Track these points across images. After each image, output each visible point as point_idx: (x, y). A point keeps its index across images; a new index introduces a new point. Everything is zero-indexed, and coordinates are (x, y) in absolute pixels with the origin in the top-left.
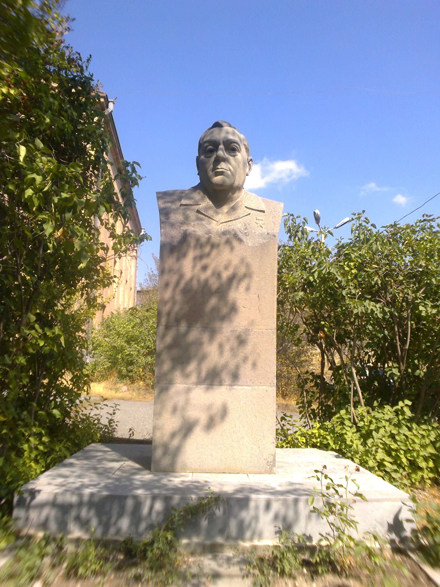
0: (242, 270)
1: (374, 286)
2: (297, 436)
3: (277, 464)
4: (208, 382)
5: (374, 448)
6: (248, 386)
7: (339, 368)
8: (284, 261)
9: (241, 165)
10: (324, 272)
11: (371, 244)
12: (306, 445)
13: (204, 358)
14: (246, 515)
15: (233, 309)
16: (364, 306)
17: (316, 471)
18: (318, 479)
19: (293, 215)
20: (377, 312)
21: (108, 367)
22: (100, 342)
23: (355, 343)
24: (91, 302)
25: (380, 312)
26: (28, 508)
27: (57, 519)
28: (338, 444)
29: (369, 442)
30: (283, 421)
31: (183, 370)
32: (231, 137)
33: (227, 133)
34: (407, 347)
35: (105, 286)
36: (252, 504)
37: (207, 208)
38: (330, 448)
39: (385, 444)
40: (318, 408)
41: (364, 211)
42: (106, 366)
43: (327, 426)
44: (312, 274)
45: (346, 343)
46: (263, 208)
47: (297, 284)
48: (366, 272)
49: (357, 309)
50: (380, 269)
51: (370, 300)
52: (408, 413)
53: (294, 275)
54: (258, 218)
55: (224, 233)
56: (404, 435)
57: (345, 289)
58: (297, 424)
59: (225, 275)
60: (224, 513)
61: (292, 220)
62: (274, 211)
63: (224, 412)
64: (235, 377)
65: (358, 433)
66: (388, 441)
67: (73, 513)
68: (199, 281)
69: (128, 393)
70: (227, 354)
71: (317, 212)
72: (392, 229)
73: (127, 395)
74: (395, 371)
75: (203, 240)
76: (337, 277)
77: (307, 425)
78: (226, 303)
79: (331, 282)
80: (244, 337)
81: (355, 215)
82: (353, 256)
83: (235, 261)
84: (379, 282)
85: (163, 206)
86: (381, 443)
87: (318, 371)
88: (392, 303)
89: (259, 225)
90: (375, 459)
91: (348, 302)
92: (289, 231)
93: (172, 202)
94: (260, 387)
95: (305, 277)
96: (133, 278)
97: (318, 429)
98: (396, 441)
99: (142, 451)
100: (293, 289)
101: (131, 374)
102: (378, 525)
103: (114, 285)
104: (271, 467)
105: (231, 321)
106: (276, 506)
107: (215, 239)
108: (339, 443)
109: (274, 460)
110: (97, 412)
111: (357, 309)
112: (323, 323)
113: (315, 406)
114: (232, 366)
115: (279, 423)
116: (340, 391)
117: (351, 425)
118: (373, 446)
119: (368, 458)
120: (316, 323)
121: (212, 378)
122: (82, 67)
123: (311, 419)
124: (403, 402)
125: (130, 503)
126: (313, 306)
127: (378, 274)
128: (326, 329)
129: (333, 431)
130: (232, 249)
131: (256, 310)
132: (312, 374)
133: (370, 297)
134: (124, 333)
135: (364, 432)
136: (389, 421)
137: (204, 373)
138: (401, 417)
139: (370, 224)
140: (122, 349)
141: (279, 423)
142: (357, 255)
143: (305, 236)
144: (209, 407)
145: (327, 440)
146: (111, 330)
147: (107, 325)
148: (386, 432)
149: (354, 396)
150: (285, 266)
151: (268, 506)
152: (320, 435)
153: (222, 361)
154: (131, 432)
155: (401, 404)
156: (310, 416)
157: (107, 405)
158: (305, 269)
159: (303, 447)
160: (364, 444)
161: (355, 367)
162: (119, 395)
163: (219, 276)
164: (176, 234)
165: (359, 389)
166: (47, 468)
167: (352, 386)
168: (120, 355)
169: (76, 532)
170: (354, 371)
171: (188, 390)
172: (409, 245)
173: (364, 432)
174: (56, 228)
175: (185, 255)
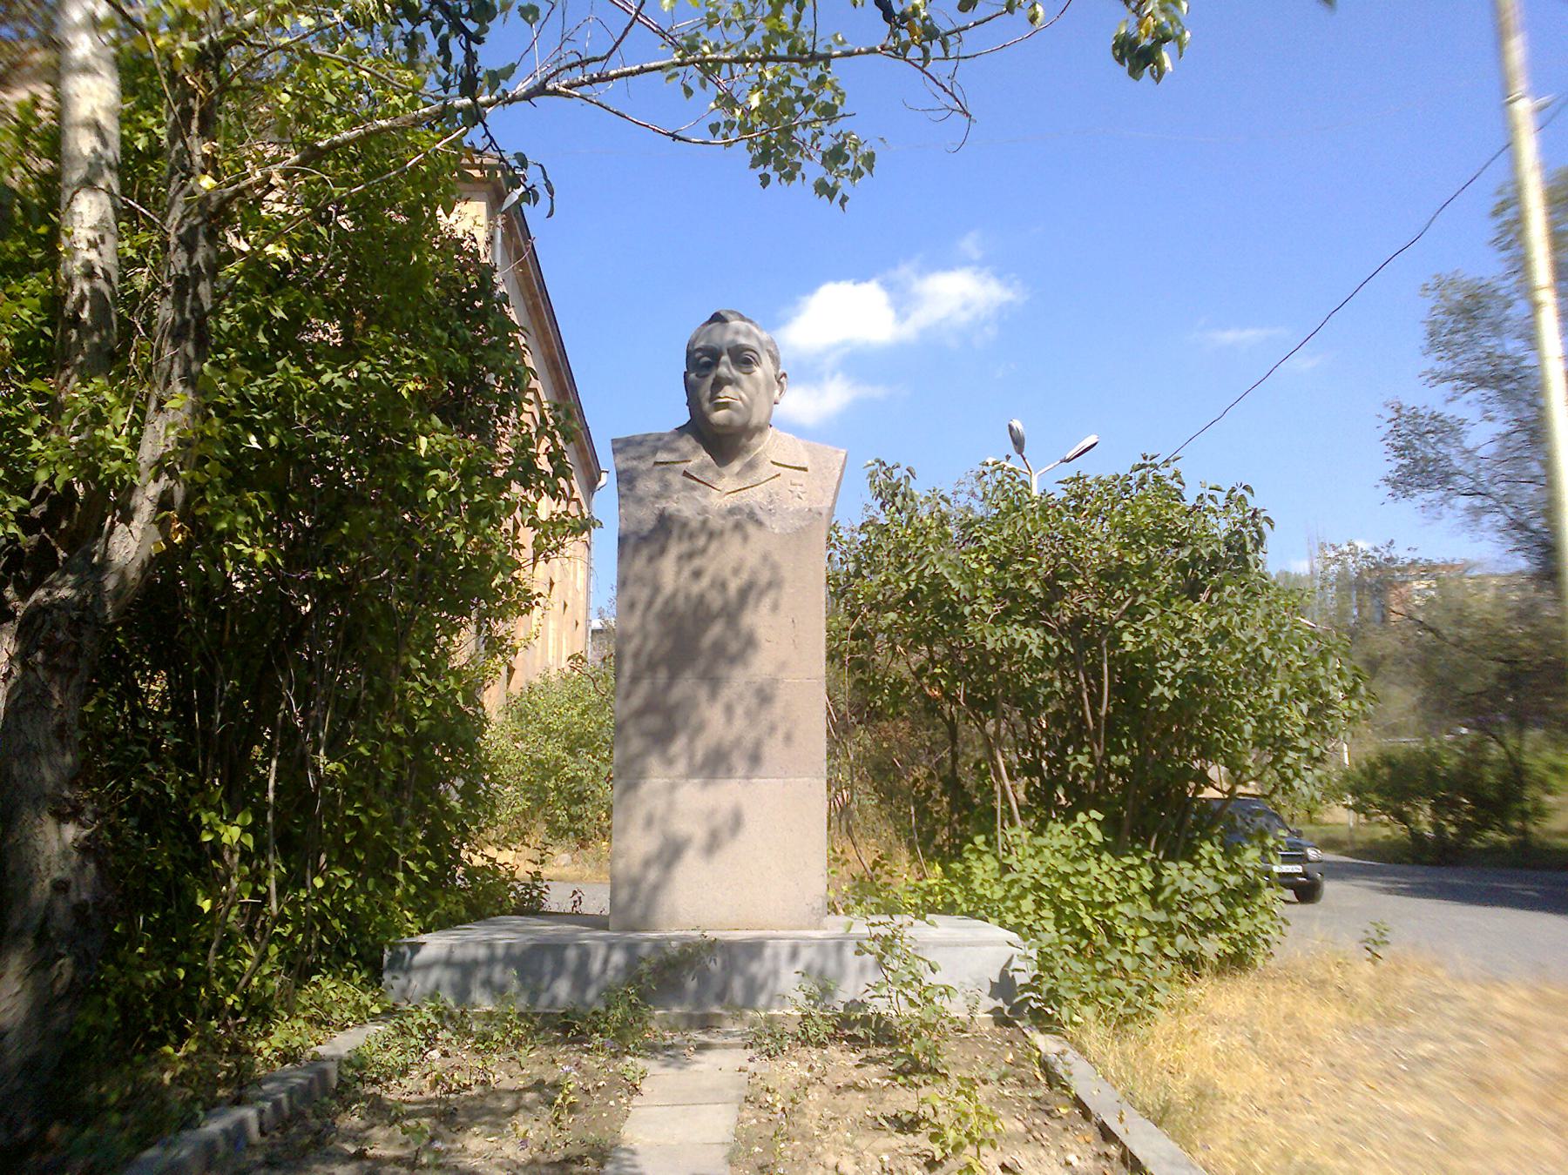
0: (764, 577)
9: (762, 389)
10: (926, 573)
13: (700, 728)
14: (757, 969)
15: (750, 642)
24: (494, 645)
26: (408, 970)
27: (454, 986)
31: (664, 752)
32: (742, 340)
33: (737, 332)
35: (521, 613)
36: (768, 952)
37: (703, 468)
46: (805, 463)
52: (1097, 836)
55: (732, 511)
59: (734, 585)
60: (724, 968)
63: (737, 822)
64: (755, 759)
67: (481, 974)
68: (687, 597)
70: (739, 723)
71: (1017, 424)
75: (695, 524)
78: (737, 634)
80: (768, 690)
83: (752, 560)
85: (623, 466)
93: (640, 458)
96: (582, 597)
101: (579, 826)
103: (537, 611)
105: (746, 665)
106: (806, 955)
107: (716, 523)
114: (748, 742)
121: (715, 765)
125: (571, 955)
130: (745, 538)
131: (792, 648)
137: (699, 756)
138: (1082, 842)
140: (558, 766)
144: (712, 813)
145: (952, 894)
146: (529, 723)
147: (520, 711)
151: (794, 954)
153: (730, 737)
163: (723, 586)
164: (646, 516)
169: (484, 1003)
171: (672, 788)
174: (468, 538)
175: (663, 551)
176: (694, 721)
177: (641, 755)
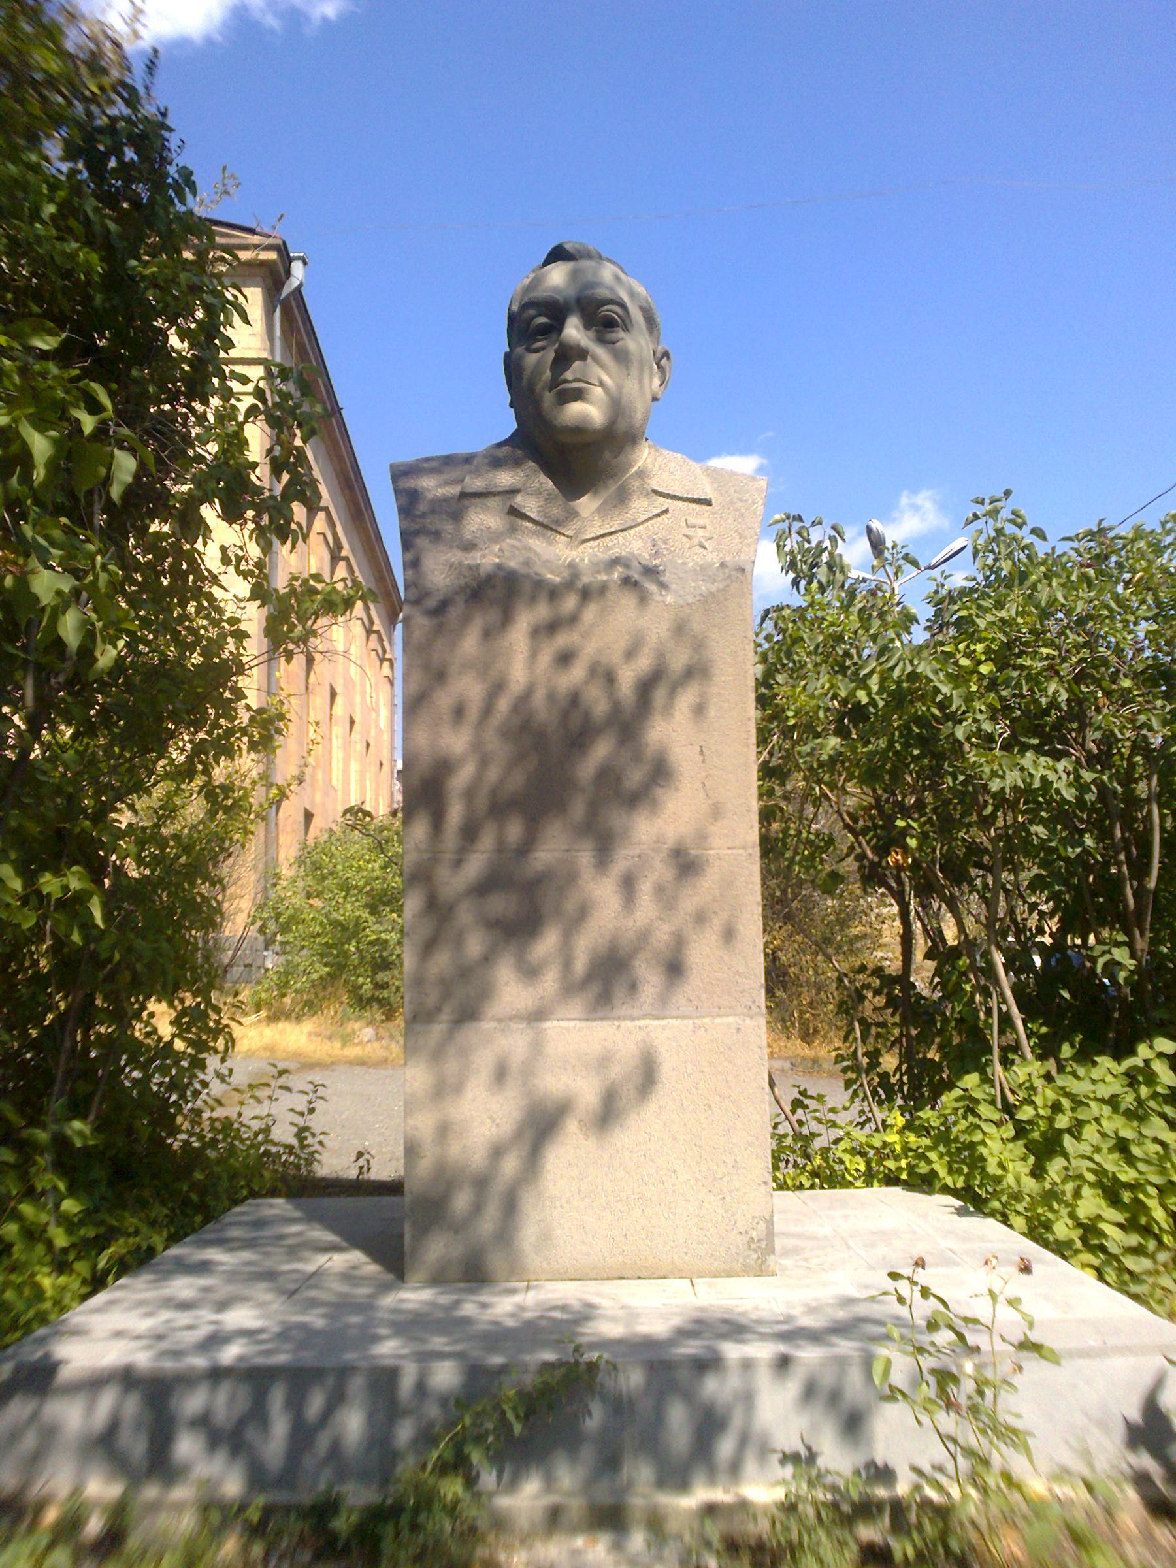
0: (678, 661)
1: (1046, 712)
2: (839, 1154)
3: (777, 1246)
4: (595, 988)
5: (1069, 1187)
6: (683, 1017)
7: (955, 953)
8: (780, 650)
10: (896, 673)
11: (1034, 587)
12: (869, 1177)
13: (583, 913)
15: (661, 771)
16: (1022, 769)
17: (894, 1276)
18: (901, 1300)
19: (800, 519)
20: (1061, 785)
21: (321, 978)
22: (296, 910)
23: (996, 879)
25: (1070, 785)
28: (959, 1172)
29: (1055, 1167)
30: (800, 1111)
34: (1152, 884)
38: (938, 1186)
39: (1100, 1172)
40: (898, 1068)
41: (1007, 493)
42: (315, 976)
43: (928, 1120)
44: (863, 683)
45: (970, 882)
47: (821, 714)
48: (1022, 668)
49: (1002, 777)
50: (1064, 660)
51: (1038, 750)
53: (810, 688)
54: (692, 521)
56: (1156, 1140)
57: (960, 722)
58: (844, 1117)
59: (628, 678)
61: (799, 533)
62: (741, 500)
63: (647, 1075)
64: (675, 969)
65: (1021, 1143)
66: (1111, 1162)
69: (376, 1045)
70: (646, 908)
72: (1092, 544)
73: (375, 1050)
74: (1121, 955)
76: (938, 684)
77: (868, 1120)
78: (637, 758)
79: (919, 705)
81: (982, 503)
82: (982, 623)
84: (1064, 696)
86: (1089, 1169)
87: (893, 966)
88: (1100, 759)
89: (696, 541)
90: (1072, 1215)
91: (973, 759)
92: (792, 566)
94: (718, 1020)
95: (843, 694)
96: (386, 737)
97: (901, 1132)
98: (1131, 1160)
99: (385, 1216)
100: (810, 729)
101: (385, 994)
102: (1095, 1431)
104: (760, 1254)
105: (655, 807)
108: (966, 1170)
109: (770, 1234)
110: (262, 1110)
111: (1002, 777)
112: (900, 823)
113: (890, 1062)
114: (662, 935)
115: (787, 1118)
116: (961, 1021)
117: (996, 1116)
118: (1067, 1179)
119: (1050, 1215)
120: (881, 827)
121: (607, 980)
122: (132, 90)
123: (880, 1103)
124: (1151, 1047)
126: (870, 777)
127: (1057, 673)
128: (912, 843)
129: (943, 1137)
131: (711, 778)
132: (878, 971)
133: (1035, 741)
134: (361, 883)
135: (1036, 1135)
136: (1112, 1101)
137: (580, 965)
138: (1144, 1091)
139: (1026, 530)
141: (787, 1118)
142: (992, 619)
143: (839, 577)
144: (604, 1061)
145: (929, 1162)
146: (324, 877)
148: (1103, 1135)
149: (1001, 1032)
150: (784, 665)
152: (906, 1149)
154: (362, 1162)
155: (1143, 1050)
156: (874, 1093)
157: (288, 1089)
158: (843, 670)
159: (859, 1183)
160: (1038, 1172)
161: (999, 948)
162: (352, 1052)
163: (610, 679)
165: (1015, 1011)
166: (97, 1283)
167: (993, 1003)
168: (354, 943)
170: (999, 959)
172: (1145, 586)
173: (1036, 1135)
175: (507, 619)
176: (570, 906)
177: (487, 959)
